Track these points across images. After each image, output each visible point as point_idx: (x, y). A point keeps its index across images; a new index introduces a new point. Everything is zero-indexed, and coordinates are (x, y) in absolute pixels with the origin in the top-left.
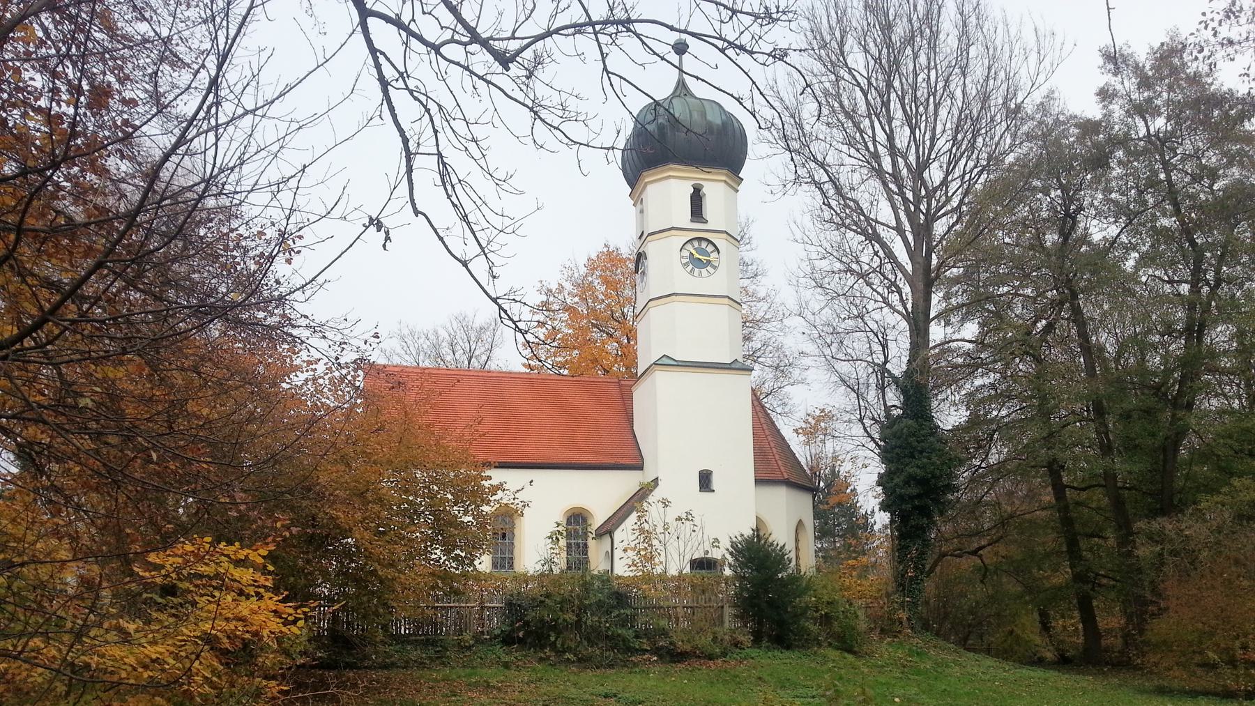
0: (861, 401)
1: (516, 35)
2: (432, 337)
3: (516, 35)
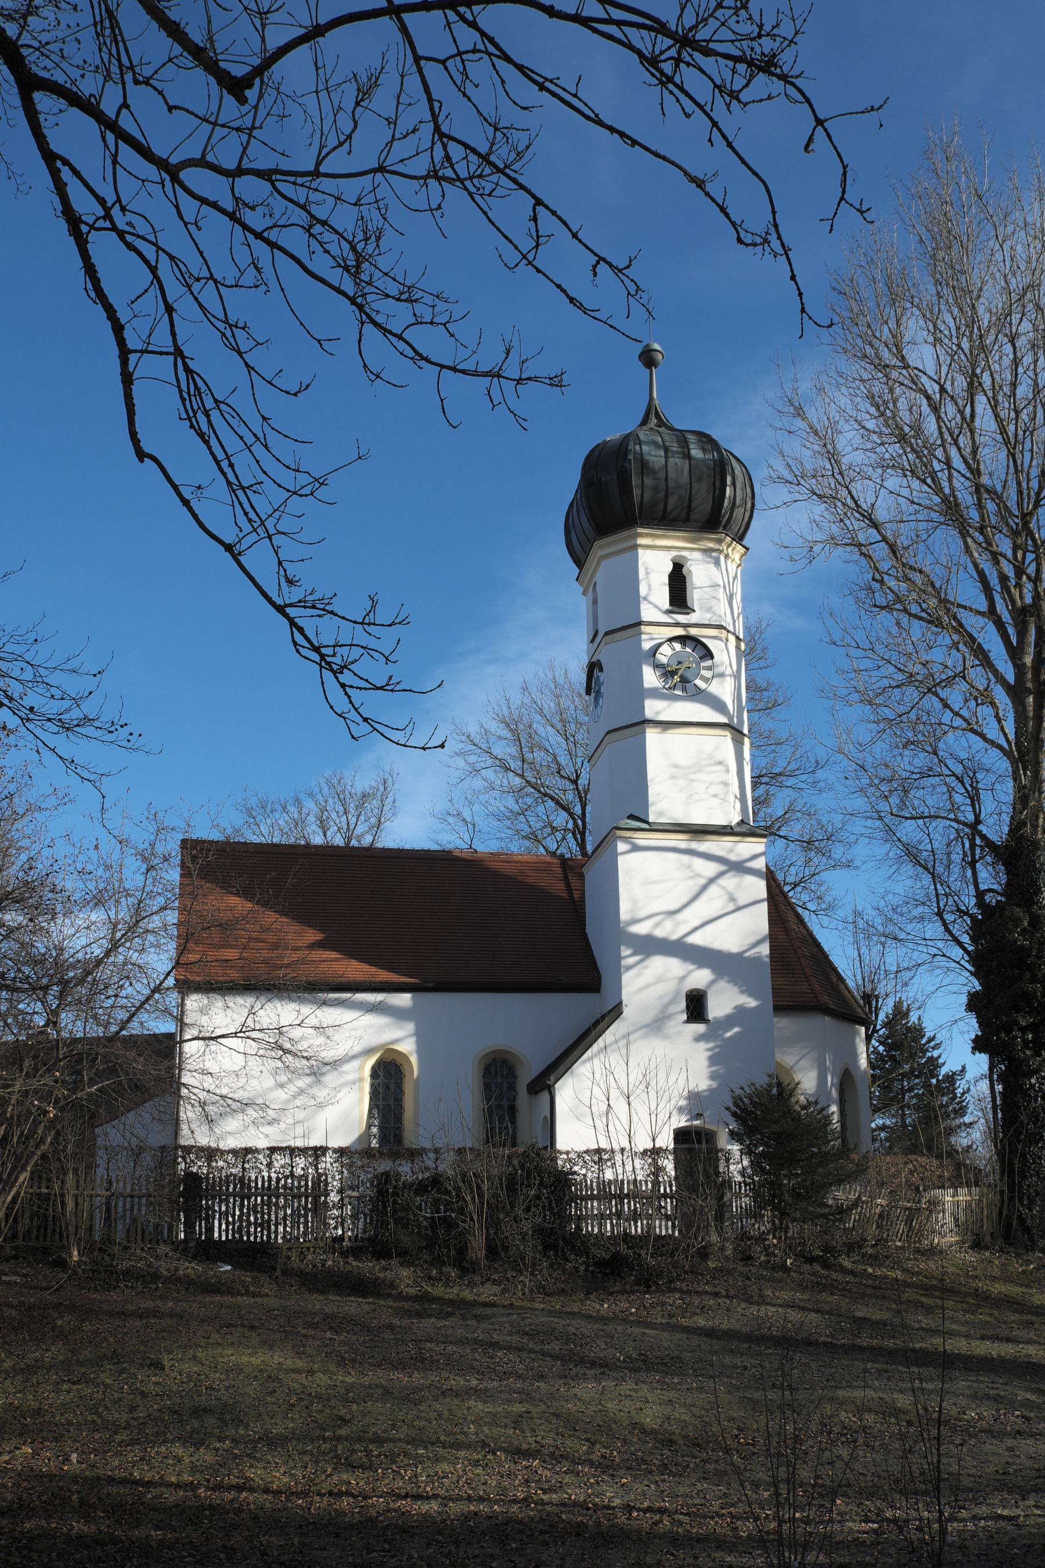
0: (939, 886)
1: (323, 169)
3: (323, 169)
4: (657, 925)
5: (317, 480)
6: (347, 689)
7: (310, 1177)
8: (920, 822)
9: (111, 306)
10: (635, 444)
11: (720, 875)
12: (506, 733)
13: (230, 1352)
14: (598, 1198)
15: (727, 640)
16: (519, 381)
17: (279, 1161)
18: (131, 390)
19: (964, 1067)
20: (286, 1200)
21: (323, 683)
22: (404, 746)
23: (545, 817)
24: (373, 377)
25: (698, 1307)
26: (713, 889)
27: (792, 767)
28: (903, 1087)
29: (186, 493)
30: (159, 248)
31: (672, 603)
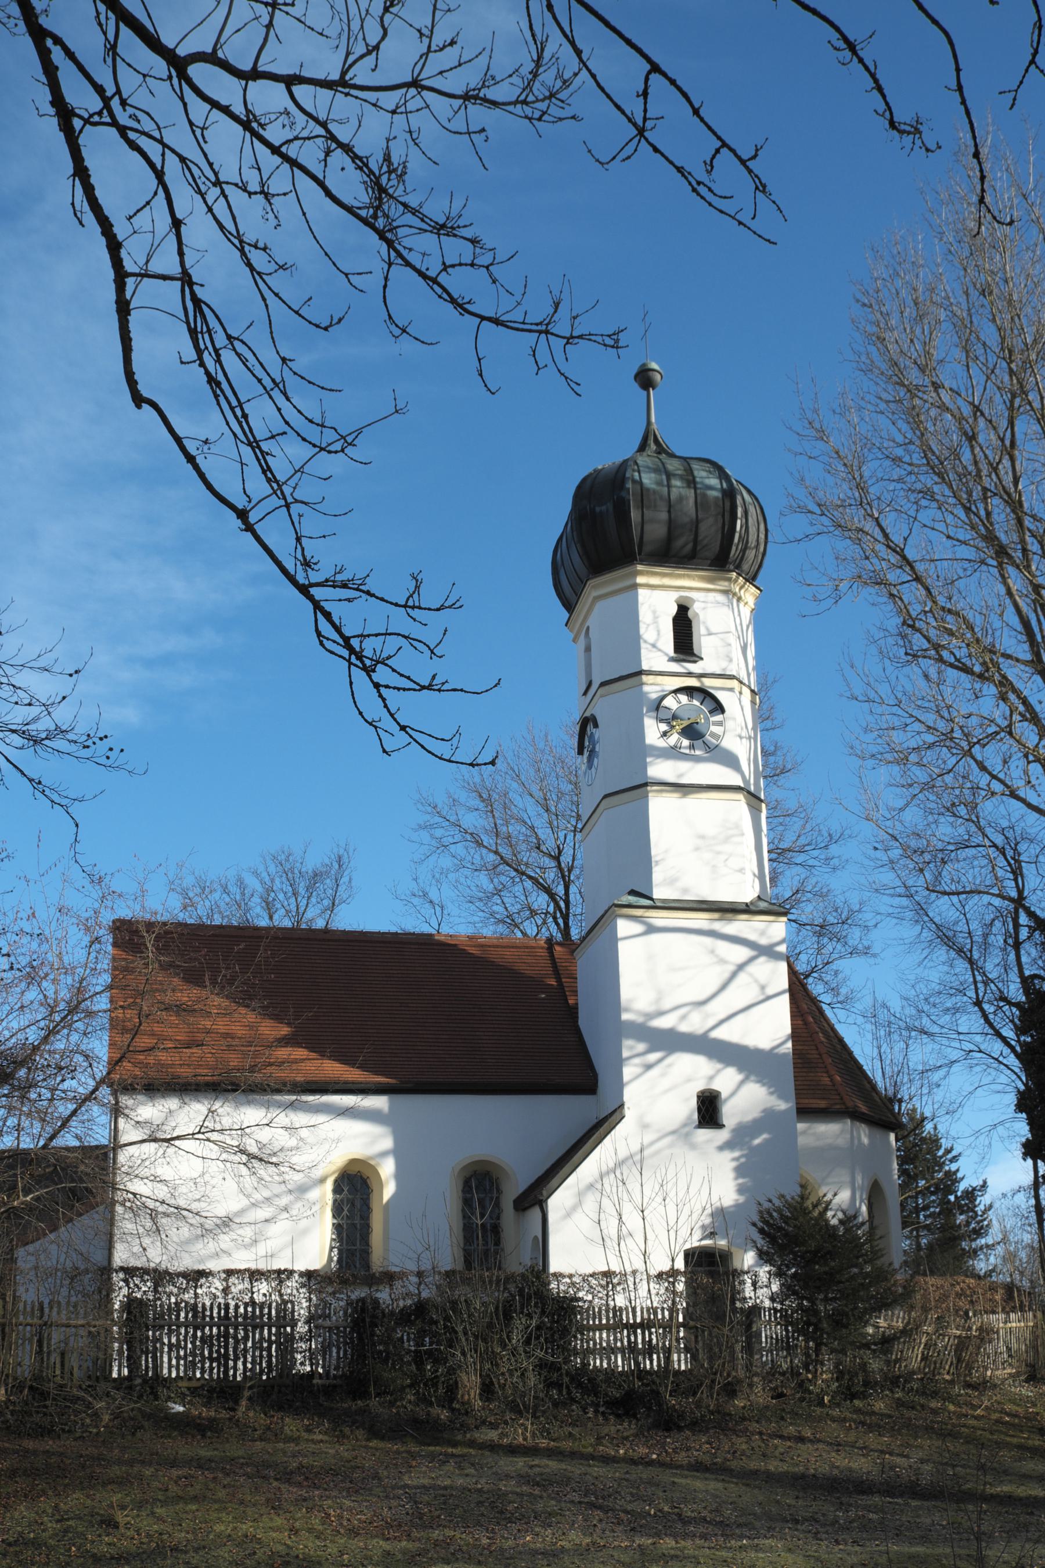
2: (234, 889)
4: (683, 1018)
5: (343, 437)
6: (382, 690)
7: (274, 1304)
8: (955, 898)
9: (107, 218)
10: (634, 471)
11: (751, 960)
12: (477, 803)
13: (194, 1508)
14: (608, 1328)
15: (741, 693)
16: (569, 340)
17: (238, 1286)
18: (127, 321)
19: (985, 1182)
20: (246, 1331)
21: (351, 683)
22: (450, 761)
23: (523, 898)
24: (397, 332)
25: (729, 1452)
26: (742, 977)
27: (803, 841)
28: (917, 1205)
29: (191, 447)
30: (165, 146)
31: (676, 651)
